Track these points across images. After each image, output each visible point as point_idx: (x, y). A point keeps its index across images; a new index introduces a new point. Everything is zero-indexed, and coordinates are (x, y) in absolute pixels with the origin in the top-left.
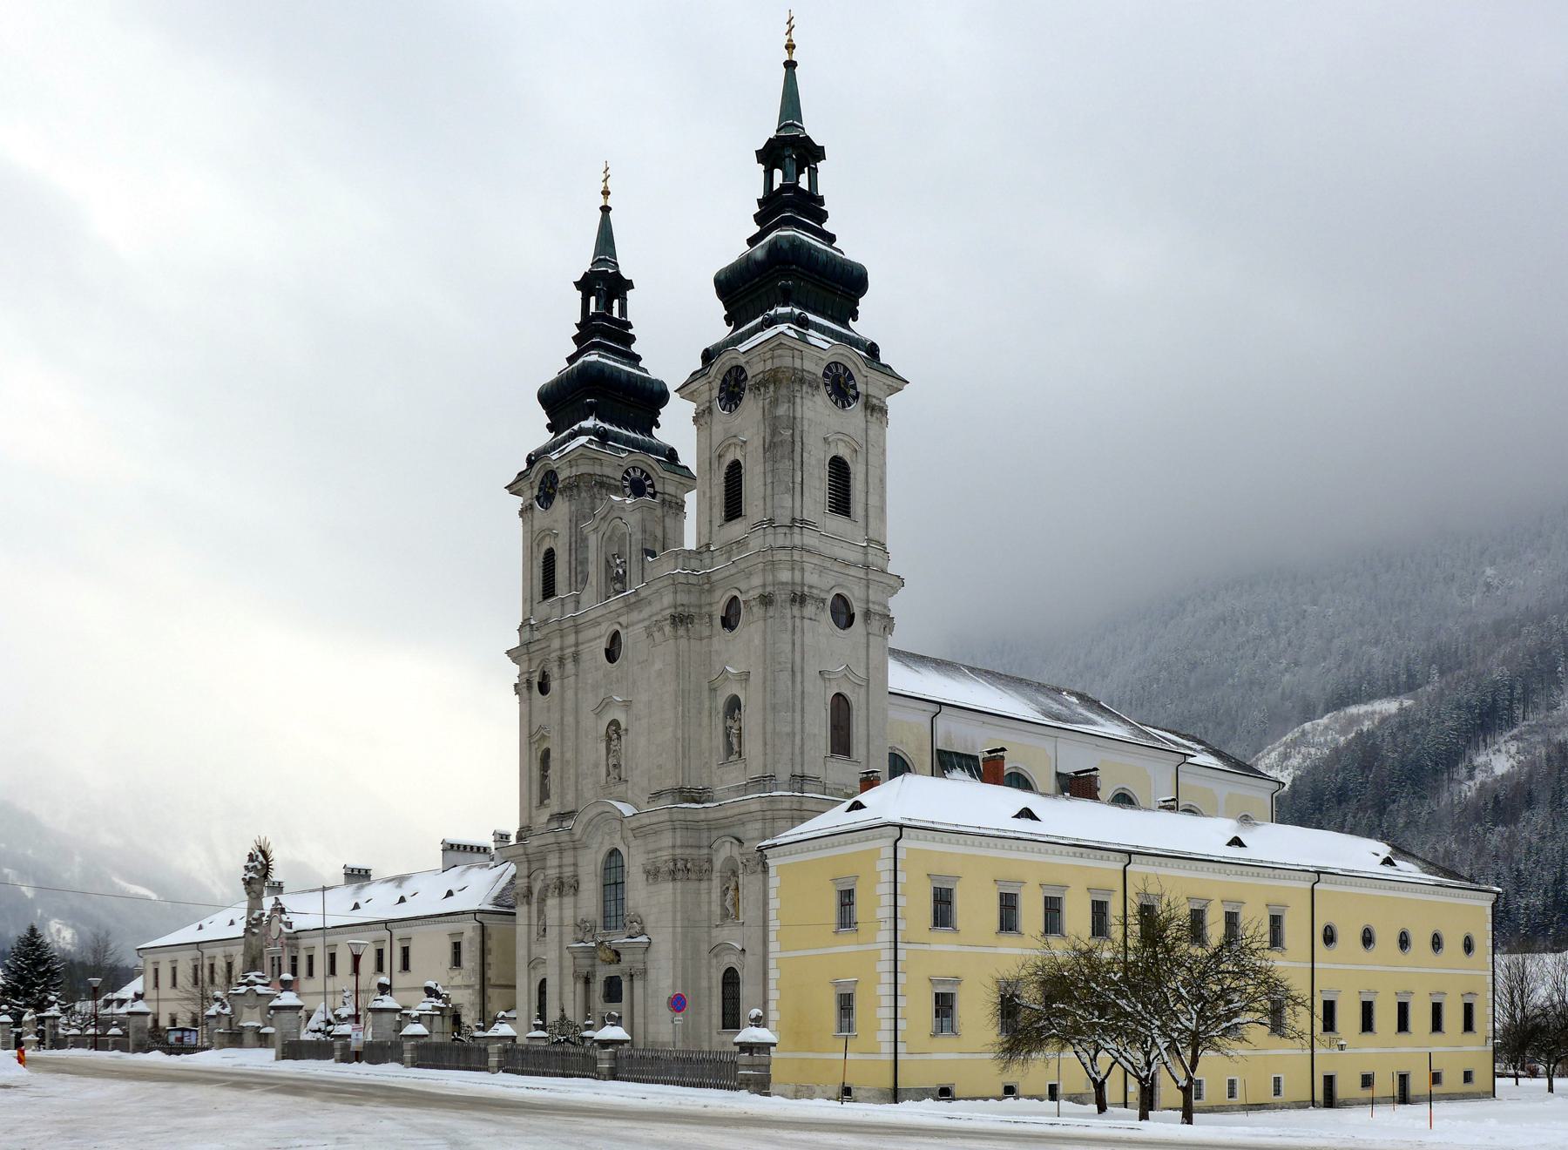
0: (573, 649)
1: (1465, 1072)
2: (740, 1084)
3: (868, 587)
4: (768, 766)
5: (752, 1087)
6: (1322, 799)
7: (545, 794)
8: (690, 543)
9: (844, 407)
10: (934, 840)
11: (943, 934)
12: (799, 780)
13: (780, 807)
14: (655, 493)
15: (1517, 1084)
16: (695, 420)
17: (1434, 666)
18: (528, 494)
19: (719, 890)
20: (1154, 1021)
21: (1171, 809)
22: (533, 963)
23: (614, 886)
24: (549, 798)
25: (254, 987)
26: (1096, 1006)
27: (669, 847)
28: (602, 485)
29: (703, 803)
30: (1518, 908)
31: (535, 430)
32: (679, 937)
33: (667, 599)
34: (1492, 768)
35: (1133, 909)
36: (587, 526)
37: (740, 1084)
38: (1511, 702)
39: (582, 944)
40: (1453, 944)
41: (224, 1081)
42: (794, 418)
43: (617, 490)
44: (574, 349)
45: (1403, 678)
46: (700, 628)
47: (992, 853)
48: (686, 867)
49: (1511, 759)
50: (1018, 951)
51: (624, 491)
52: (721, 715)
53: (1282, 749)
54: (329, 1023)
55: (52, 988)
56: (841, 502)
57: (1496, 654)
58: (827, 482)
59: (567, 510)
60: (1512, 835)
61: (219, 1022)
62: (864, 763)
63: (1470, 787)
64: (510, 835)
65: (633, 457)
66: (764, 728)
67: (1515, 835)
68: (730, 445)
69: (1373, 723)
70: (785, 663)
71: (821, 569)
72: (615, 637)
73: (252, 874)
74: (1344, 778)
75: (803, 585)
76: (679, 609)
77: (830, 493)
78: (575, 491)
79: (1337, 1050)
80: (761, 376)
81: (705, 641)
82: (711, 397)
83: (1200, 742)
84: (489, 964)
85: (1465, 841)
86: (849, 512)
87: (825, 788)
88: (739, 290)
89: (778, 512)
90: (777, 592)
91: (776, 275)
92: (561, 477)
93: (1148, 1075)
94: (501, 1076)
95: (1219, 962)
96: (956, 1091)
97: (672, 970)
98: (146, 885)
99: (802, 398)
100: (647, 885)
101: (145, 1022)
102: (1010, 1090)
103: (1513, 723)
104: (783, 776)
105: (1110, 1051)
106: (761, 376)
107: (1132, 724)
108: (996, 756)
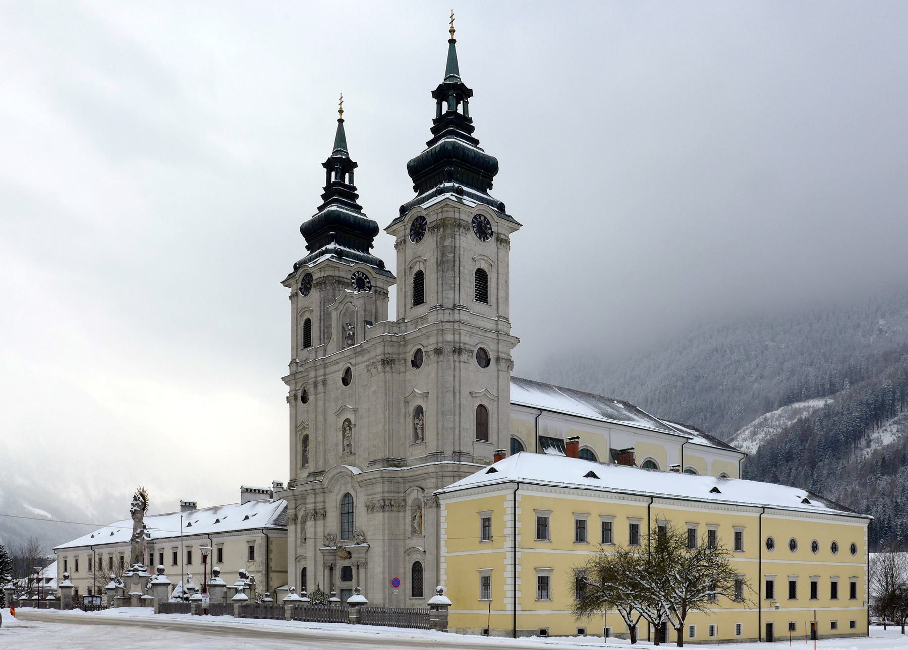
0: (323, 377)
1: (851, 622)
2: (431, 626)
3: (498, 343)
4: (440, 446)
5: (438, 627)
6: (776, 459)
7: (305, 461)
8: (392, 317)
9: (484, 240)
10: (537, 490)
11: (542, 543)
12: (458, 455)
13: (447, 470)
14: (371, 286)
15: (885, 629)
16: (396, 247)
17: (846, 379)
18: (295, 287)
19: (410, 517)
20: (661, 593)
21: (677, 471)
22: (298, 559)
23: (347, 515)
24: (307, 462)
25: (138, 573)
26: (630, 584)
27: (380, 492)
28: (339, 282)
29: (400, 467)
30: (896, 525)
31: (299, 249)
32: (386, 544)
33: (379, 350)
34: (881, 441)
35: (653, 526)
36: (331, 307)
37: (431, 626)
38: (893, 401)
39: (329, 548)
40: (844, 548)
41: (138, 625)
42: (455, 247)
43: (348, 285)
44: (322, 202)
45: (827, 386)
46: (400, 367)
47: (571, 497)
48: (390, 504)
49: (893, 436)
50: (586, 553)
51: (352, 285)
52: (411, 417)
53: (752, 429)
54: (185, 593)
55: (5, 572)
56: (482, 295)
57: (885, 372)
58: (474, 283)
59: (319, 297)
60: (893, 481)
61: (117, 592)
62: (496, 443)
63: (868, 452)
64: (282, 484)
65: (357, 266)
66: (437, 424)
67: (895, 481)
68: (417, 261)
69: (809, 413)
70: (450, 387)
71: (471, 333)
72: (348, 371)
73: (136, 508)
74: (791, 447)
75: (460, 342)
76: (387, 356)
77: (476, 290)
78: (323, 286)
79: (774, 609)
80: (435, 222)
81: (402, 374)
82: (405, 234)
83: (696, 430)
84: (271, 559)
85: (864, 485)
86: (487, 301)
87: (473, 459)
88: (422, 172)
89: (445, 300)
90: (445, 347)
91: (444, 164)
92: (315, 277)
93: (659, 622)
94: (293, 622)
95: (699, 560)
96: (550, 632)
97: (382, 563)
98: (43, 509)
99: (459, 235)
100: (367, 514)
101: (70, 592)
102: (581, 632)
103: (894, 413)
104: (449, 452)
105: (638, 609)
106: (435, 222)
107: (655, 420)
108: (574, 441)
